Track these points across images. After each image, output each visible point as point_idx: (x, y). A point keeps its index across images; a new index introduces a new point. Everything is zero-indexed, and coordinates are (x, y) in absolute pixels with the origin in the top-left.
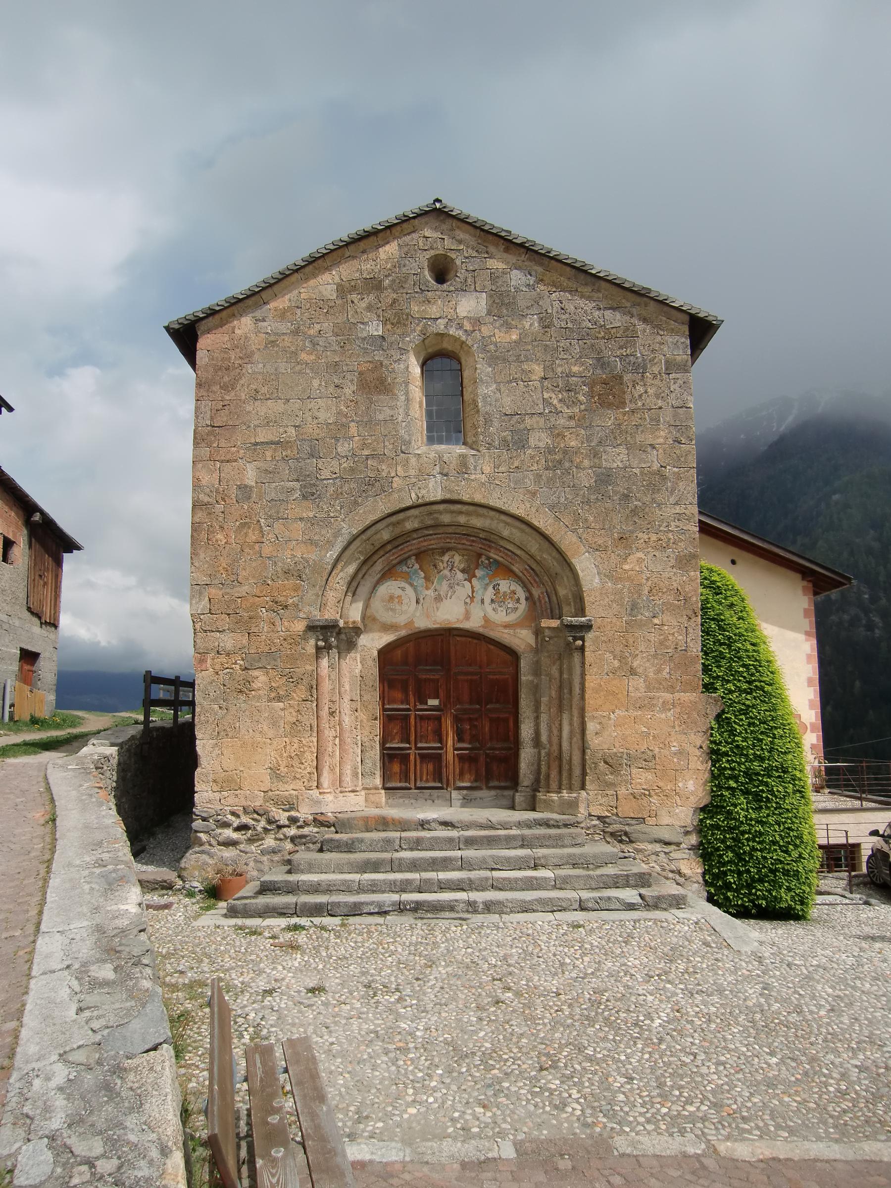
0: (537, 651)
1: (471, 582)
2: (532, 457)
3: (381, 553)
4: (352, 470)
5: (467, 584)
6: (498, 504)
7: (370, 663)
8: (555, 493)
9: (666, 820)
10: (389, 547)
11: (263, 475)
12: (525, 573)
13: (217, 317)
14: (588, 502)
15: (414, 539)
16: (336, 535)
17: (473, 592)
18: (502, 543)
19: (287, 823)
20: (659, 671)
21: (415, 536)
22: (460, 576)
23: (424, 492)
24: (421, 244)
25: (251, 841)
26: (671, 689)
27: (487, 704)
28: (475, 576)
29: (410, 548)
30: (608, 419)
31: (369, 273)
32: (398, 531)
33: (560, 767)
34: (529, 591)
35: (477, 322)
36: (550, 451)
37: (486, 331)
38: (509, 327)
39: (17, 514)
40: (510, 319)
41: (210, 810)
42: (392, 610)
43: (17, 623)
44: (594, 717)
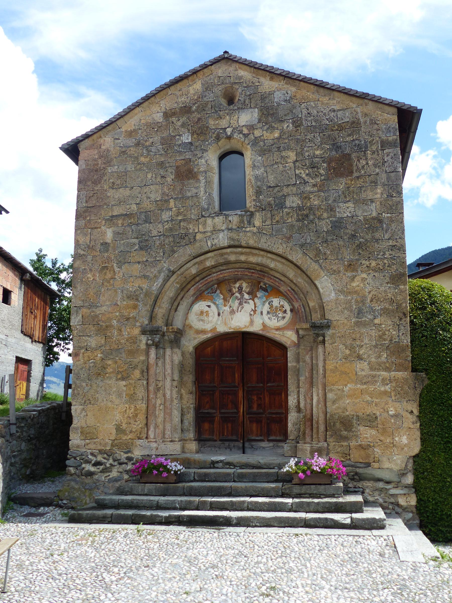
0: (298, 345)
1: (254, 301)
2: (288, 214)
3: (193, 283)
4: (171, 229)
5: (251, 301)
6: (265, 246)
7: (188, 356)
8: (303, 237)
9: (387, 465)
10: (198, 279)
11: (116, 236)
12: (288, 292)
13: (90, 139)
14: (326, 241)
15: (214, 273)
16: (160, 272)
17: (255, 307)
18: (272, 272)
19: (126, 461)
20: (380, 357)
21: (214, 270)
22: (246, 296)
23: (216, 241)
24: (216, 81)
25: (103, 471)
26: (388, 369)
27: (267, 383)
28: (257, 297)
29: (211, 279)
30: (341, 184)
31: (183, 103)
32: (201, 267)
33: (312, 425)
34: (292, 305)
35: (251, 127)
36: (300, 208)
37: (257, 133)
38: (272, 129)
39: (15, 274)
40: (273, 124)
41: (77, 452)
42: (202, 320)
43: (14, 340)
44: (331, 390)
